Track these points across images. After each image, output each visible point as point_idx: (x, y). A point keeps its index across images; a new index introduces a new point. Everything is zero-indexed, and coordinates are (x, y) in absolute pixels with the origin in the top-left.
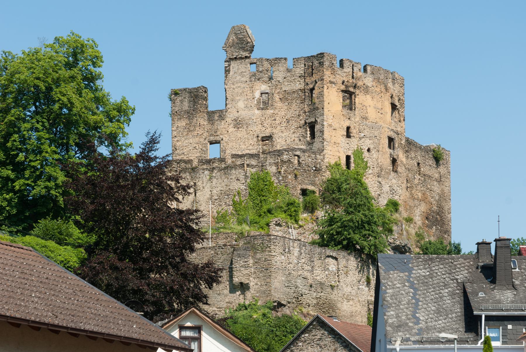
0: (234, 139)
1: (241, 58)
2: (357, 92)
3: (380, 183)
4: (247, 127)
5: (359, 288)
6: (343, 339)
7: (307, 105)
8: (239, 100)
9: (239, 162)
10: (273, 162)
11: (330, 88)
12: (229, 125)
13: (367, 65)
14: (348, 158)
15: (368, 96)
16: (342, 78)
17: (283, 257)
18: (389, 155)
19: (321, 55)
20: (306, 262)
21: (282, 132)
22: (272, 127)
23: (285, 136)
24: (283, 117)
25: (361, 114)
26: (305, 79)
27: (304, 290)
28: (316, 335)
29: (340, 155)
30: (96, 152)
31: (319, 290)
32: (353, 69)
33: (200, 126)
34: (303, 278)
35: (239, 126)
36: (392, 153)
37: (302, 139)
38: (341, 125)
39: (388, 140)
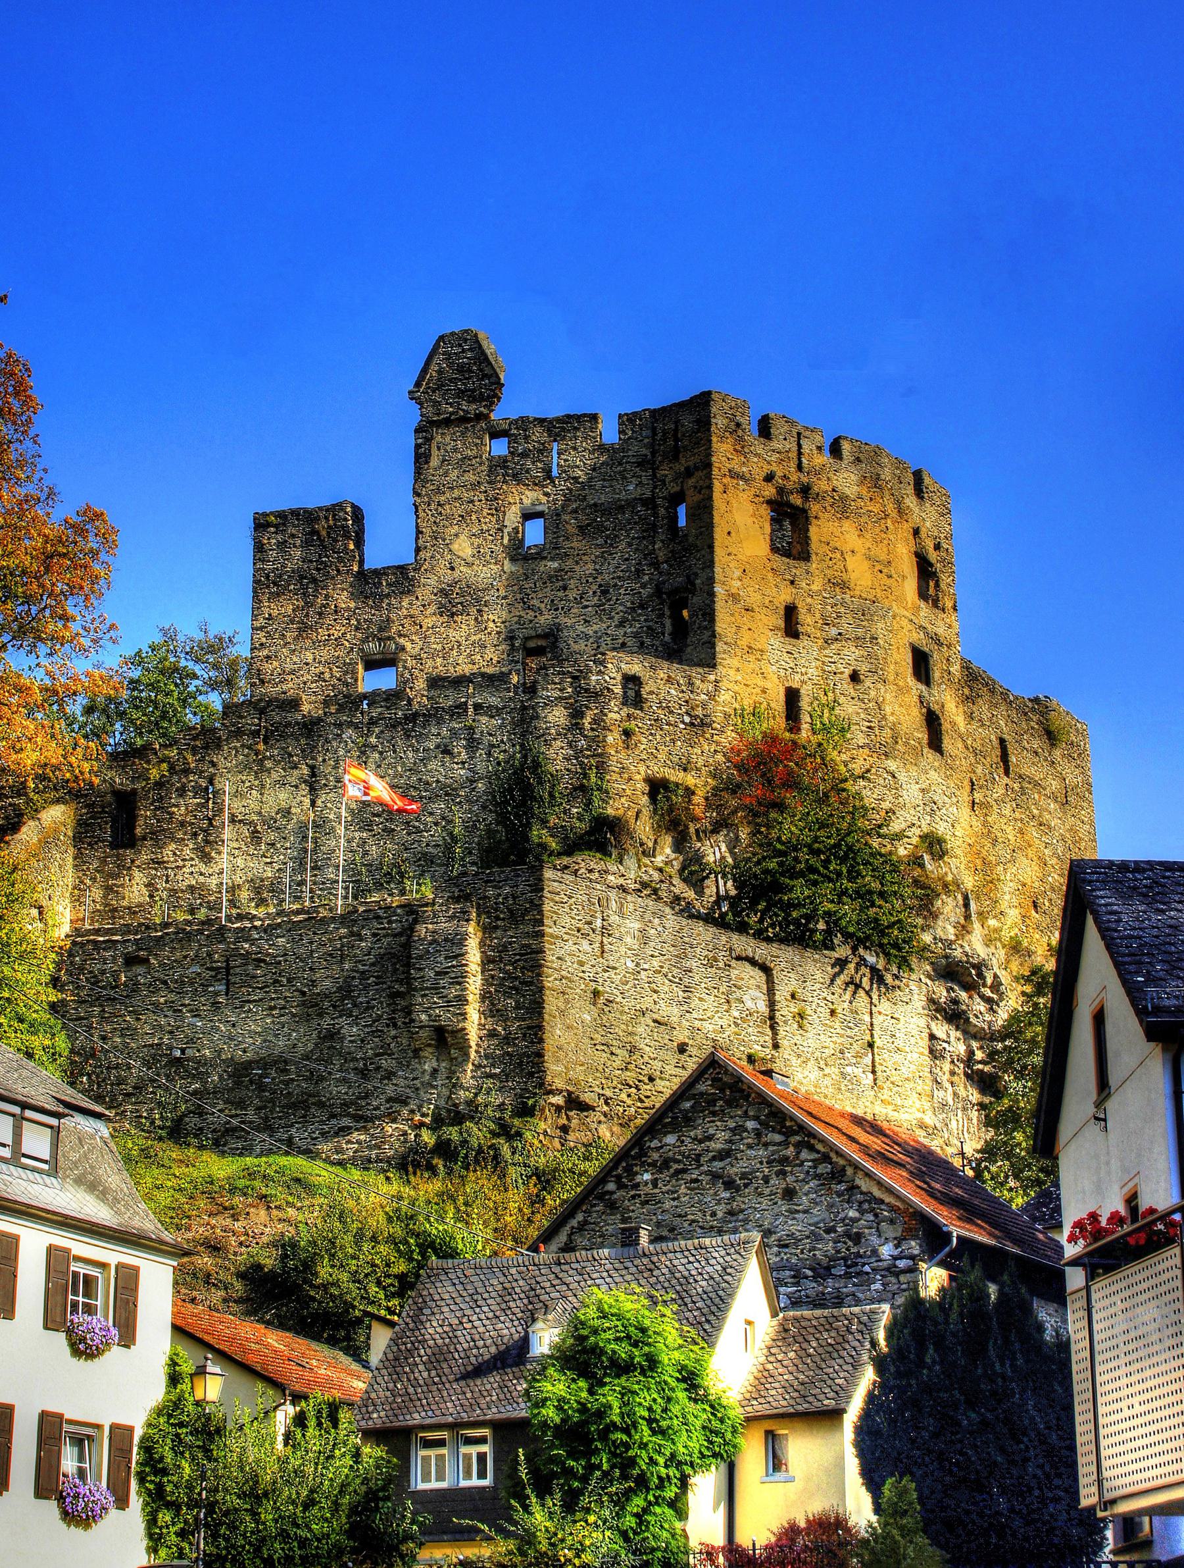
0: (439, 647)
1: (464, 420)
2: (814, 508)
3: (894, 777)
4: (479, 611)
5: (843, 1075)
6: (820, 1147)
7: (662, 541)
8: (456, 535)
9: (447, 700)
10: (557, 694)
11: (731, 490)
12: (424, 606)
13: (839, 437)
14: (792, 696)
15: (847, 525)
17: (585, 945)
18: (916, 699)
19: (702, 401)
20: (665, 970)
21: (586, 621)
22: (556, 610)
23: (596, 632)
24: (590, 580)
25: (829, 572)
26: (654, 470)
27: (657, 1065)
28: (710, 1138)
29: (768, 685)
32: (800, 446)
33: (336, 612)
34: (655, 1021)
35: (454, 610)
37: (648, 641)
39: (910, 655)
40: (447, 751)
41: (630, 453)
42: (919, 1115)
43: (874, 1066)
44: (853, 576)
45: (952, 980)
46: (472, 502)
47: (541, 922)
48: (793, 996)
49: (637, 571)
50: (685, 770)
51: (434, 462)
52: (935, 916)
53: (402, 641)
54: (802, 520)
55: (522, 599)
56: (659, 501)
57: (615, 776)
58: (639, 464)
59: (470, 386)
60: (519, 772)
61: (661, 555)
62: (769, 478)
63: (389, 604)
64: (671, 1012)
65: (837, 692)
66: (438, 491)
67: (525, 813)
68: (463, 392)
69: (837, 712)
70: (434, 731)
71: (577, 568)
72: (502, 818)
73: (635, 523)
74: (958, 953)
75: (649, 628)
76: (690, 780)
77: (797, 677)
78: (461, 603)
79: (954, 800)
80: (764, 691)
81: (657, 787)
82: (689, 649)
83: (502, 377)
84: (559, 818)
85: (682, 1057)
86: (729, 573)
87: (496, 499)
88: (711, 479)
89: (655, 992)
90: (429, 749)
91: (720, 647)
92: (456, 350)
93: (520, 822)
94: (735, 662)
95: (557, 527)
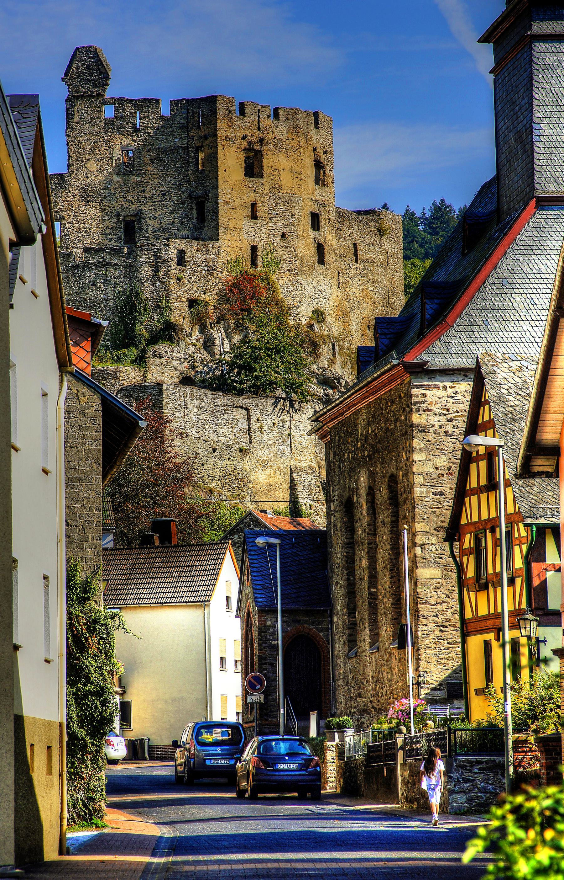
0: (82, 218)
1: (91, 96)
2: (265, 149)
10: (146, 260)
11: (226, 147)
12: (73, 196)
14: (254, 249)
15: (281, 155)
16: (243, 131)
18: (312, 240)
21: (155, 209)
22: (140, 202)
23: (160, 215)
25: (272, 182)
26: (188, 132)
30: (540, 778)
31: (225, 456)
32: (259, 117)
36: (317, 236)
37: (185, 221)
38: (243, 202)
40: (94, 285)
41: (176, 122)
42: (310, 463)
43: (291, 444)
44: (284, 182)
45: (326, 385)
46: (96, 142)
47: (162, 408)
48: (258, 420)
49: (180, 185)
50: (205, 293)
51: (76, 119)
52: (318, 356)
53: (63, 214)
54: (259, 155)
55: (123, 196)
56: (190, 149)
57: (174, 301)
58: (180, 128)
59: (93, 78)
60: (129, 297)
61: (192, 178)
62: (244, 138)
63: (55, 194)
64: (210, 436)
65: (275, 244)
66: (79, 135)
67: (133, 318)
68: (90, 81)
69: (274, 254)
70: (88, 274)
71: (150, 181)
72: (122, 319)
73: (179, 159)
74: (329, 374)
75: (186, 215)
76: (208, 299)
77: (256, 239)
78: (92, 196)
79: (330, 285)
80: (241, 250)
81: (192, 303)
82: (206, 229)
83: (109, 74)
84: (148, 321)
85: (215, 454)
86: (225, 191)
87: (109, 141)
88: (217, 143)
89: (204, 428)
90: (85, 283)
91: (221, 230)
92: (85, 57)
93: (131, 322)
94: (227, 237)
95: (140, 159)
